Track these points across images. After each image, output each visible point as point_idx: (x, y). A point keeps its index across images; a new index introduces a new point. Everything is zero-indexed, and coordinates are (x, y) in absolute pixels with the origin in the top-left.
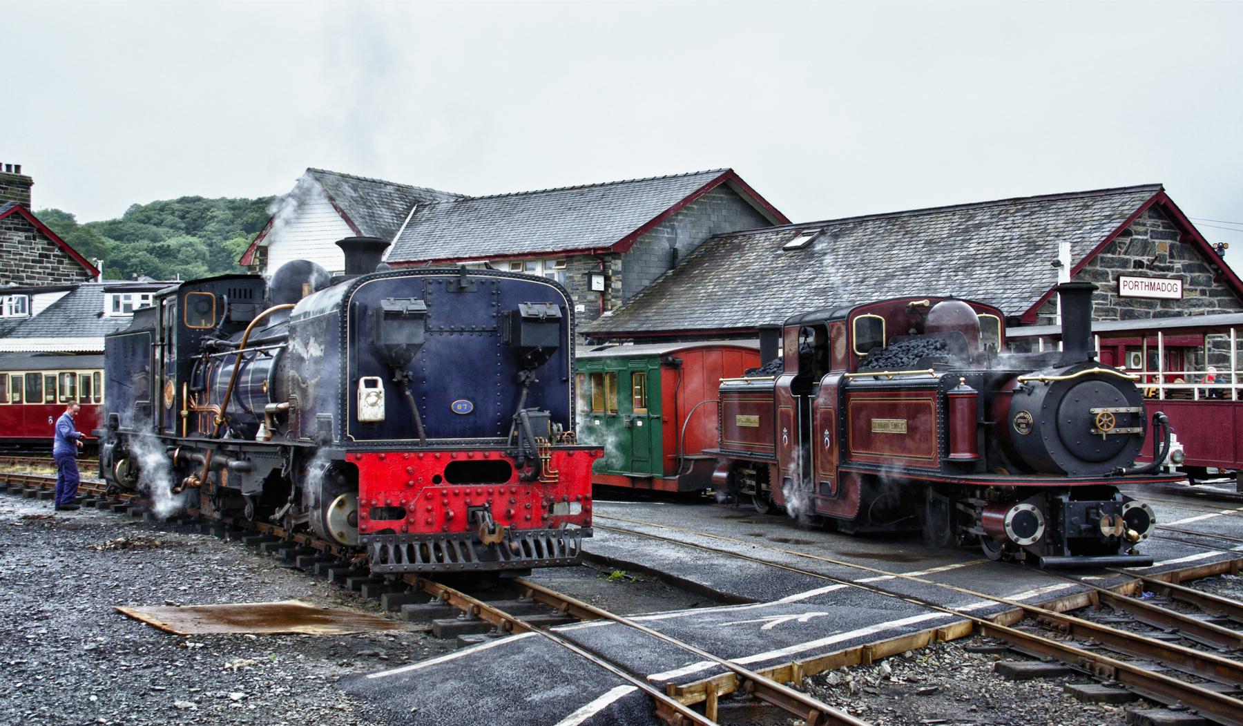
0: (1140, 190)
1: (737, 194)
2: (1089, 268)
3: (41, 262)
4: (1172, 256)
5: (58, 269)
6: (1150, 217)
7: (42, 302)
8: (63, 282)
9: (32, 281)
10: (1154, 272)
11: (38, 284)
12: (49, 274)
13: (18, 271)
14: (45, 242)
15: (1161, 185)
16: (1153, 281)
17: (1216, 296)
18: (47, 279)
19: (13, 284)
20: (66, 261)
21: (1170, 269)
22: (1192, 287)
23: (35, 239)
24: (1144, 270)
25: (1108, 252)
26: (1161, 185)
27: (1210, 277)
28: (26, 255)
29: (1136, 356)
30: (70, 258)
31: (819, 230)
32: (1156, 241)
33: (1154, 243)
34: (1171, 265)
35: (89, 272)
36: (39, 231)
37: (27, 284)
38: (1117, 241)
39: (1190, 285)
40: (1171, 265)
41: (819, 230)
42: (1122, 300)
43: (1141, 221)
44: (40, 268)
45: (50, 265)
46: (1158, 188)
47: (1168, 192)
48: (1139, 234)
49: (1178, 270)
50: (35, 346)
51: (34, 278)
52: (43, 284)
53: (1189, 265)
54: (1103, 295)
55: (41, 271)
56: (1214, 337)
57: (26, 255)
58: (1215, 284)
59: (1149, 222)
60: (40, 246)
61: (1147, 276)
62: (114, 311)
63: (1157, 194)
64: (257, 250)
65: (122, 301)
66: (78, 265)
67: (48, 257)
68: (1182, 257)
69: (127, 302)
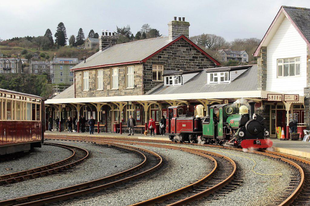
20: (205, 59)
30: (207, 58)
65: (214, 76)
66: (210, 61)
67: (196, 58)
69: (216, 76)
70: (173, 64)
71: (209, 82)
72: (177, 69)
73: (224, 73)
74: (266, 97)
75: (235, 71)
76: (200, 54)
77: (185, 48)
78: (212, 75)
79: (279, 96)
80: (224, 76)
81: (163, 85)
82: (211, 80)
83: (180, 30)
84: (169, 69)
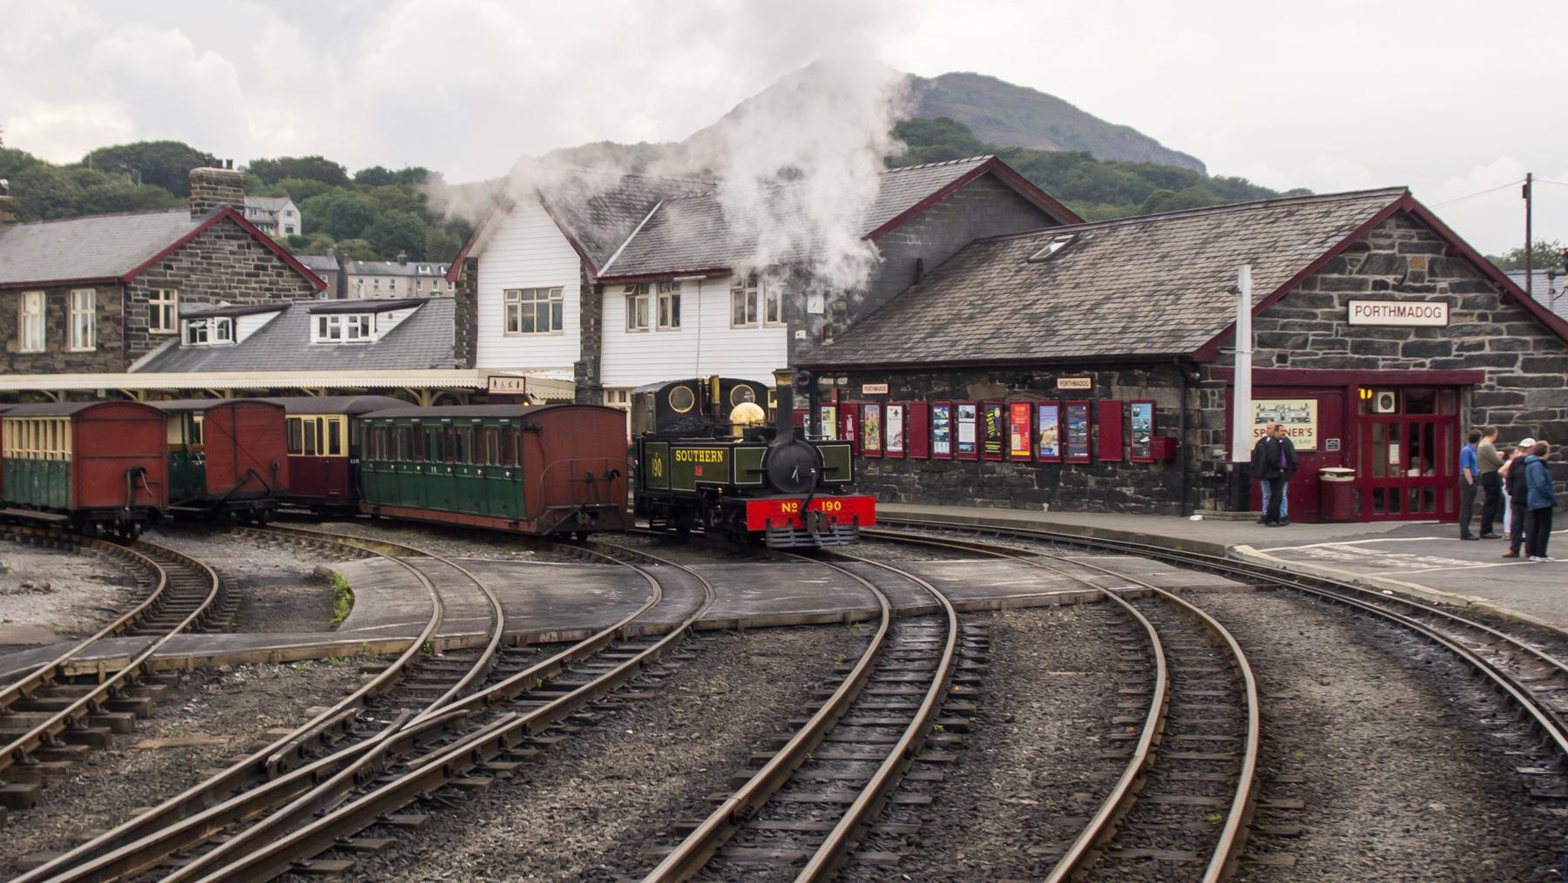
0: (1385, 193)
1: (1007, 187)
2: (1301, 292)
3: (258, 276)
4: (1432, 273)
5: (277, 283)
6: (1398, 227)
7: (248, 326)
8: (283, 298)
9: (246, 299)
10: (1404, 294)
11: (253, 303)
12: (267, 290)
13: (230, 287)
14: (261, 251)
15: (1406, 188)
16: (1402, 305)
17: (1505, 321)
18: (264, 296)
19: (224, 304)
20: (286, 273)
21: (1432, 289)
22: (1465, 311)
23: (249, 248)
24: (1390, 292)
25: (1333, 272)
26: (1406, 188)
27: (1494, 298)
28: (240, 267)
29: (1386, 398)
30: (291, 269)
31: (1071, 236)
32: (1408, 255)
33: (1405, 258)
34: (1432, 284)
35: (314, 286)
36: (254, 237)
37: (241, 302)
38: (1347, 258)
39: (1462, 307)
40: (1432, 284)
41: (1071, 236)
42: (1353, 329)
43: (1384, 232)
44: (256, 282)
45: (267, 279)
46: (1402, 192)
47: (1417, 195)
48: (1380, 247)
49: (1443, 290)
50: (373, 380)
51: (248, 295)
52: (259, 302)
53: (1460, 283)
54: (1325, 324)
55: (257, 286)
56: (1501, 372)
57: (240, 267)
58: (1503, 306)
59: (1397, 233)
60: (255, 257)
61: (1392, 299)
62: (350, 337)
63: (1400, 200)
64: (464, 262)
65: (329, 324)
66: (301, 276)
67: (265, 268)
68: (1447, 274)
69: (335, 325)
70: (203, 287)
71: (315, 337)
72: (213, 299)
73: (359, 316)
74: (485, 386)
75: (386, 314)
76: (275, 259)
77: (235, 243)
78: (323, 322)
79: (514, 381)
80: (359, 324)
81: (179, 343)
82: (323, 331)
83: (222, 195)
84: (194, 301)
